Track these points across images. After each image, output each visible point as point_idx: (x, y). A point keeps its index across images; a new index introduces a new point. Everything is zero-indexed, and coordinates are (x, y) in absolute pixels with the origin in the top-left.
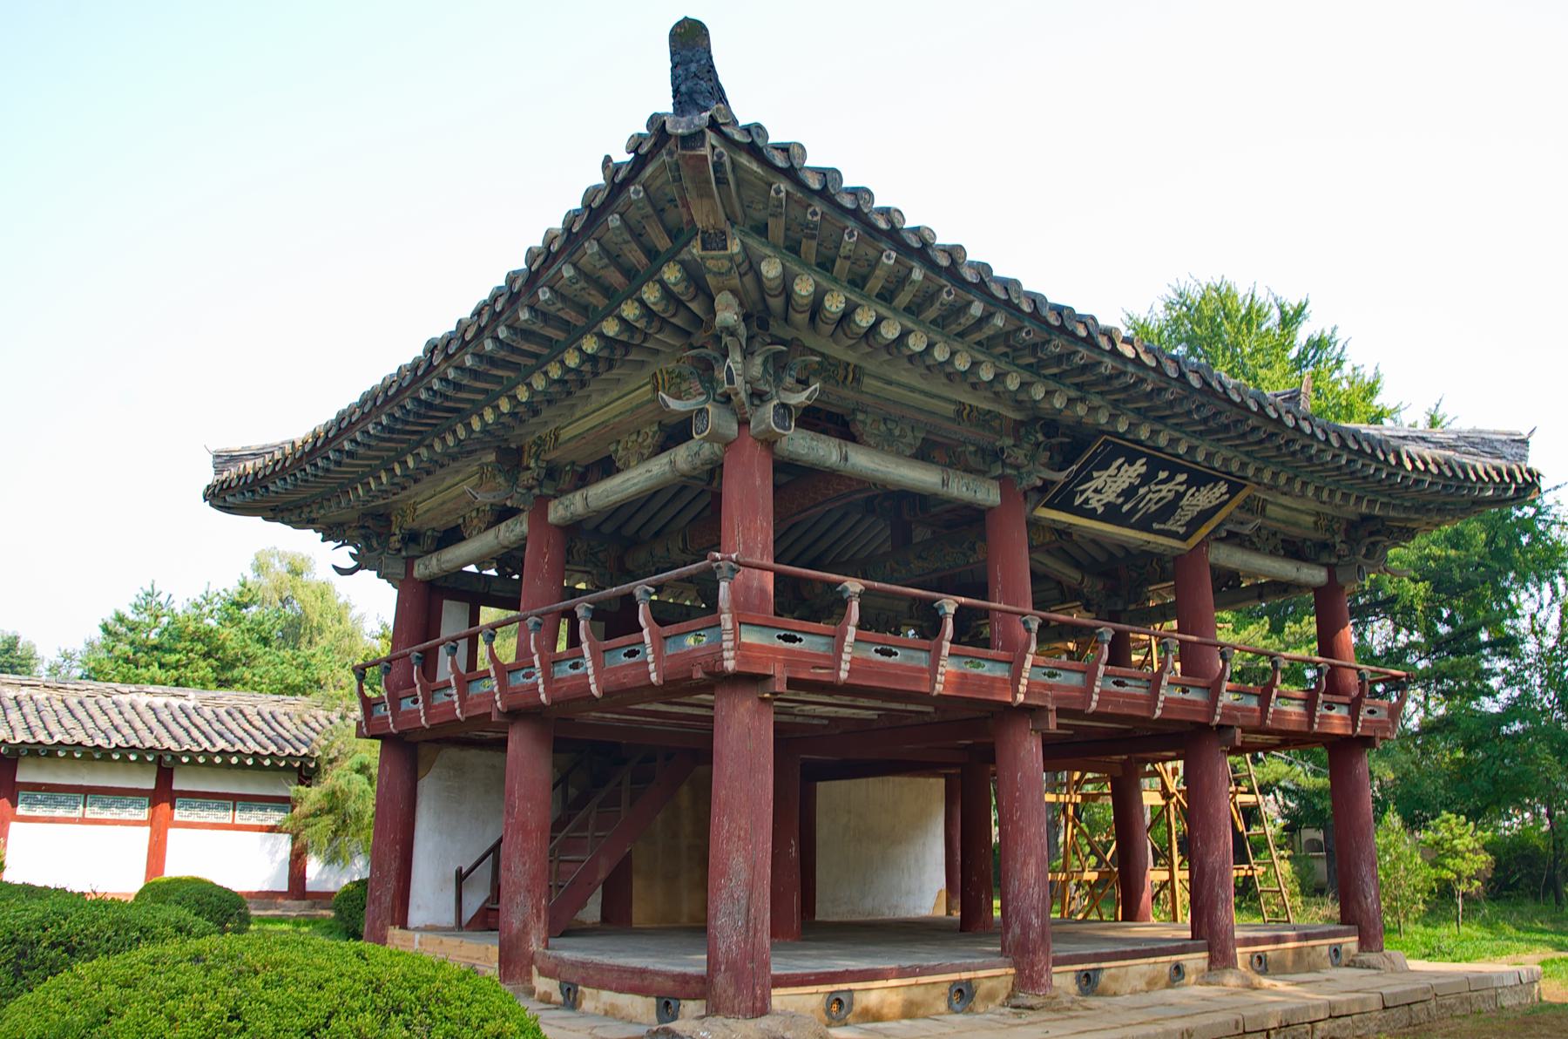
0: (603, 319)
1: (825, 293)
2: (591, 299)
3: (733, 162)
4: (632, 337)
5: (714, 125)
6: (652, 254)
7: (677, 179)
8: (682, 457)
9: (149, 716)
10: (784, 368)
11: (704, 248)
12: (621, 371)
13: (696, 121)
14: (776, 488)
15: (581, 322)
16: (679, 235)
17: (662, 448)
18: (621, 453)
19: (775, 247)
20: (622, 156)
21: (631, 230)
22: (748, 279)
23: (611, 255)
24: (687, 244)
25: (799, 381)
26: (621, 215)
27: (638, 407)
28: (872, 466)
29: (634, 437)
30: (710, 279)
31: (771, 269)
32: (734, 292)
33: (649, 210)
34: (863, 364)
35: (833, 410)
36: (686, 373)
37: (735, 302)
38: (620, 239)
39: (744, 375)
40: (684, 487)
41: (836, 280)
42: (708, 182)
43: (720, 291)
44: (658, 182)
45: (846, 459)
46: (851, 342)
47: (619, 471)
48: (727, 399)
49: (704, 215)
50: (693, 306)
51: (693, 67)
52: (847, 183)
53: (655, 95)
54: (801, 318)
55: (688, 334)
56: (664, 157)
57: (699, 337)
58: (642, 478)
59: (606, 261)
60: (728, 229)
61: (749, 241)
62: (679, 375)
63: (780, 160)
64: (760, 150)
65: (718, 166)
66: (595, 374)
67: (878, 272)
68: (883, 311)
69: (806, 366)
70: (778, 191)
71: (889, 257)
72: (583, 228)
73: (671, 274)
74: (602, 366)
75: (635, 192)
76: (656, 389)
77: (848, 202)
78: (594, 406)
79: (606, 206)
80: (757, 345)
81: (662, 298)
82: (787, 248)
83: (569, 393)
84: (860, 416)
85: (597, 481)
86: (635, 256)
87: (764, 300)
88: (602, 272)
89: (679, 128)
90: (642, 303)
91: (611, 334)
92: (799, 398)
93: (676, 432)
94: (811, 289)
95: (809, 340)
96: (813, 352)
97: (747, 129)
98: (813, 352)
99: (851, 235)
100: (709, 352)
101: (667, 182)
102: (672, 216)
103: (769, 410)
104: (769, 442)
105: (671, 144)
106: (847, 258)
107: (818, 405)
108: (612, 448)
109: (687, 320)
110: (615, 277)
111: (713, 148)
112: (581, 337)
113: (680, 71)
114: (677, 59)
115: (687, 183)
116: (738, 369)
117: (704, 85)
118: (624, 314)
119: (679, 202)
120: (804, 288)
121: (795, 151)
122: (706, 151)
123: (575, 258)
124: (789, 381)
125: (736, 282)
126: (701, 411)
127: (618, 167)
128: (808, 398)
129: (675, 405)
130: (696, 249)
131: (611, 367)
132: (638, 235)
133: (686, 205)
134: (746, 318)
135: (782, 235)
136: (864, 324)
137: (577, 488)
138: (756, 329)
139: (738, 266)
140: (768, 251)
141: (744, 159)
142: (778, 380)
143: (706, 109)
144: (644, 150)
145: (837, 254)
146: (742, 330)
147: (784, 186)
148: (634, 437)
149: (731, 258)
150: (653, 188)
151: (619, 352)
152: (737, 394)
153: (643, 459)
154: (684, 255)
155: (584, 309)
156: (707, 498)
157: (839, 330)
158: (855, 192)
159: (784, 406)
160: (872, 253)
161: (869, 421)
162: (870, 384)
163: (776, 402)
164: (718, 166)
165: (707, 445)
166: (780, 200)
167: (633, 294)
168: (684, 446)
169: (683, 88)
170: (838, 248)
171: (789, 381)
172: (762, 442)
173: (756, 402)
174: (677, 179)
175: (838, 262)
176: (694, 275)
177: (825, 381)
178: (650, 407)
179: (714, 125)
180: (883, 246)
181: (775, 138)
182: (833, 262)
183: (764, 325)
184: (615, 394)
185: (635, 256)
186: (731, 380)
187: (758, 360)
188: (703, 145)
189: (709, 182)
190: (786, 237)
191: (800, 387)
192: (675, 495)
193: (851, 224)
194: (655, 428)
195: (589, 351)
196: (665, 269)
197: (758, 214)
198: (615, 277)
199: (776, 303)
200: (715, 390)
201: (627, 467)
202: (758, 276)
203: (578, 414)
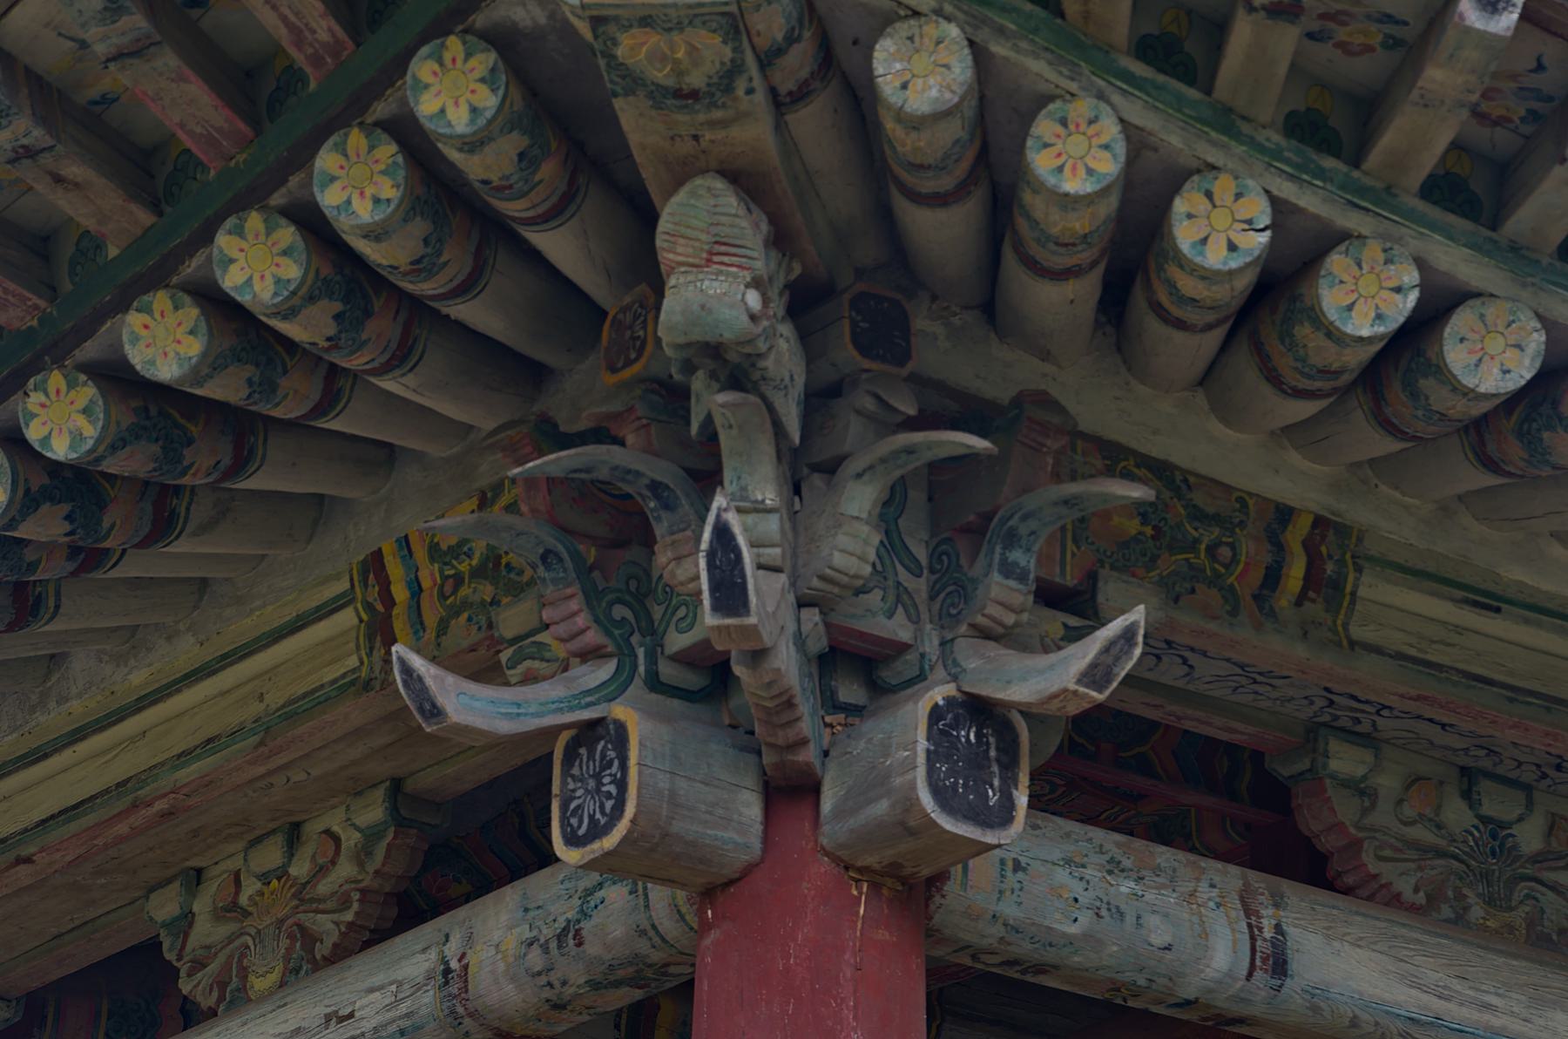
45: (1279, 966)
68: (1458, 262)
93: (475, 833)
103: (907, 731)
128: (1095, 675)
163: (939, 694)
173: (850, 691)
187: (860, 497)
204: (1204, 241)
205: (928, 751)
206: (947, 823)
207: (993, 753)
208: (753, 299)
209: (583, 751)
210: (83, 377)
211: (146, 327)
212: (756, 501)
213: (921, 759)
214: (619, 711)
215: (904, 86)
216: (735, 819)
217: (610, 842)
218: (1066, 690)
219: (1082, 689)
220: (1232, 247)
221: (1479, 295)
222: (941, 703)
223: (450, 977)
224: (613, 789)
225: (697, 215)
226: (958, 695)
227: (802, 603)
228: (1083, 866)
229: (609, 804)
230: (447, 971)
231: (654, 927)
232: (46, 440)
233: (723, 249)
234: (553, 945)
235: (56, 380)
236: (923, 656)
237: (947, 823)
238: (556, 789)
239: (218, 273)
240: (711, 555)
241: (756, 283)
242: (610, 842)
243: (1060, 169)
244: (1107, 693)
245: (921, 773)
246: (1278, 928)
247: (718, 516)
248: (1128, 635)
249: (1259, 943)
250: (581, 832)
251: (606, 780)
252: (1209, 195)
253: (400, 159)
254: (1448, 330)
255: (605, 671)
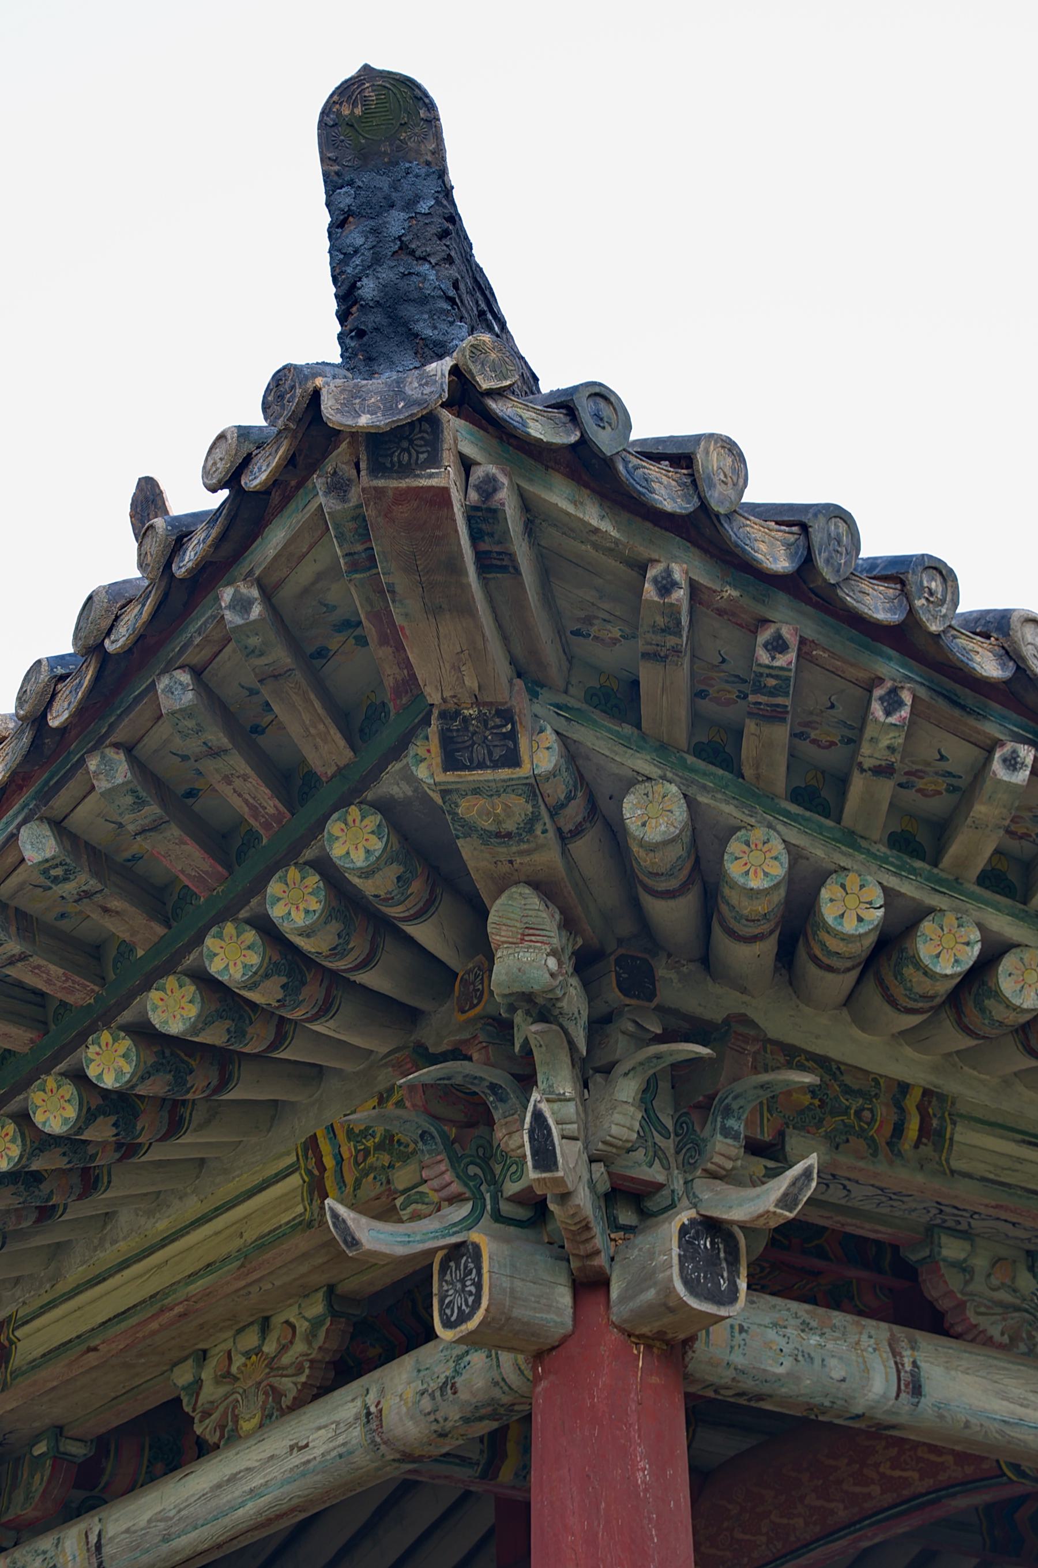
0: (146, 987)
1: (822, 877)
2: (110, 925)
3: (522, 496)
4: (239, 1034)
5: (465, 396)
6: (294, 783)
7: (364, 562)
8: (401, 1396)
10: (705, 1107)
11: (451, 763)
12: (210, 1136)
13: (413, 388)
14: (702, 1478)
15: (79, 993)
16: (374, 725)
17: (341, 1370)
18: (210, 1392)
19: (663, 749)
20: (191, 496)
21: (410, 274)
22: (587, 849)
23: (172, 795)
24: (399, 749)
25: (754, 1148)
26: (197, 673)
27: (264, 1243)
28: (1000, 1408)
29: (250, 1339)
30: (469, 850)
31: (654, 816)
32: (544, 888)
33: (280, 656)
34: (951, 1086)
35: (866, 1230)
36: (407, 1135)
37: (548, 919)
38: (193, 746)
39: (584, 1136)
40: (406, 1487)
41: (851, 839)
42: (454, 566)
43: (502, 885)
44: (306, 573)
45: (917, 1389)
46: (915, 1020)
47: (203, 1450)
48: (535, 1212)
49: (447, 661)
50: (423, 933)
51: (396, 223)
52: (874, 545)
53: (296, 318)
54: (751, 957)
55: (412, 1016)
56: (320, 496)
57: (445, 1024)
58: (275, 1472)
59: (153, 810)
60: (520, 702)
61: (585, 736)
62: (388, 1142)
63: (666, 492)
64: (607, 463)
65: (483, 519)
66: (128, 1150)
67: (980, 810)
69: (774, 1100)
70: (666, 586)
71: (1012, 763)
72: (84, 714)
73: (354, 842)
74: (147, 1127)
75: (236, 604)
76: (317, 1189)
77: (877, 604)
78: (124, 1247)
79: (148, 647)
80: (619, 1044)
81: (330, 914)
82: (699, 751)
83: (46, 1213)
84: (952, 1249)
85: (133, 1487)
86: (242, 791)
87: (635, 905)
88: (142, 845)
89: (359, 409)
90: (269, 931)
91: (175, 1027)
92: (757, 1203)
93: (384, 1320)
94: (778, 870)
95: (778, 1020)
96: (794, 1056)
97: (564, 405)
98: (794, 1056)
99: (892, 703)
100: (477, 1070)
101: (332, 572)
102: (351, 668)
103: (665, 1241)
104: (671, 1344)
105: (339, 459)
106: (883, 771)
107: (817, 1218)
108: (183, 1376)
109: (409, 980)
110: (181, 857)
111: (466, 465)
112: (81, 1040)
113: (355, 236)
114: (346, 198)
115: (391, 573)
116: (570, 1122)
117: (432, 277)
118: (215, 968)
119: (369, 629)
120: (756, 866)
121: (710, 461)
122: (446, 476)
123: (60, 802)
124: (723, 1149)
125: (548, 857)
126: (456, 1251)
127: (182, 532)
128: (787, 1200)
129: (379, 1238)
130: (425, 767)
131: (175, 1127)
132: (248, 731)
133: (392, 638)
134: (585, 963)
135: (683, 713)
136: (946, 967)
137: (70, 1512)
138: (613, 995)
139: (554, 812)
140: (642, 763)
141: (559, 496)
142: (690, 1149)
143: (440, 351)
144: (256, 478)
145: (853, 762)
146: (574, 1000)
147: (683, 567)
148: (250, 1339)
149: (532, 788)
150: (287, 592)
151: (199, 1083)
152: (565, 1197)
153: (280, 1409)
154: (391, 785)
155: (90, 955)
156: (482, 1518)
157: (870, 987)
158: (897, 573)
159: (712, 1226)
160: (960, 754)
161: (980, 1263)
162: (975, 1146)
163: (685, 1216)
164: (483, 519)
165: (478, 1359)
166: (673, 611)
167: (242, 905)
168: (407, 1362)
169: (368, 288)
170: (853, 741)
171: (723, 1149)
172: (648, 1342)
173: (626, 1217)
174: (364, 562)
175: (858, 784)
176: (424, 847)
177: (835, 1143)
178: (301, 1243)
179: (465, 396)
180: (992, 729)
181: (648, 424)
182: (842, 783)
183: (639, 982)
184: (192, 1207)
185: (242, 791)
186: (545, 1157)
187: (627, 1089)
188: (434, 460)
189: (462, 572)
190: (696, 717)
191: (759, 1165)
192: (381, 1512)
193: (890, 668)
194: (317, 1308)
195: (109, 1082)
196: (334, 827)
197: (610, 654)
198: (181, 857)
199: (674, 915)
200: (496, 1184)
201: (230, 1436)
202: (615, 834)
203: (75, 1273)
204: (842, 916)
205: (679, 1255)
206: (694, 1303)
207: (722, 1255)
208: (552, 963)
209: (452, 1264)
210: (122, 1034)
211: (162, 1000)
212: (560, 1094)
213: (675, 1261)
214: (475, 1236)
215: (644, 825)
216: (555, 1306)
217: (472, 1325)
218: (768, 1212)
219: (779, 1211)
220: (860, 919)
221: (1018, 946)
222: (687, 1222)
223: (370, 1417)
224: (473, 1289)
225: (513, 911)
226: (698, 1217)
227: (592, 1160)
228: (785, 1327)
229: (471, 1300)
230: (369, 1414)
231: (503, 1379)
232: (100, 1076)
233: (531, 932)
234: (438, 1394)
235: (106, 1036)
236: (673, 1191)
237: (694, 1303)
238: (435, 1290)
239: (207, 963)
240: (531, 1132)
241: (553, 953)
242: (472, 1325)
243: (747, 873)
244: (796, 1212)
245: (676, 1270)
246: (914, 1364)
247: (535, 1106)
248: (807, 1173)
249: (902, 1374)
250: (453, 1319)
251: (468, 1283)
252: (843, 886)
253: (321, 884)
254: (1000, 969)
255: (466, 1209)
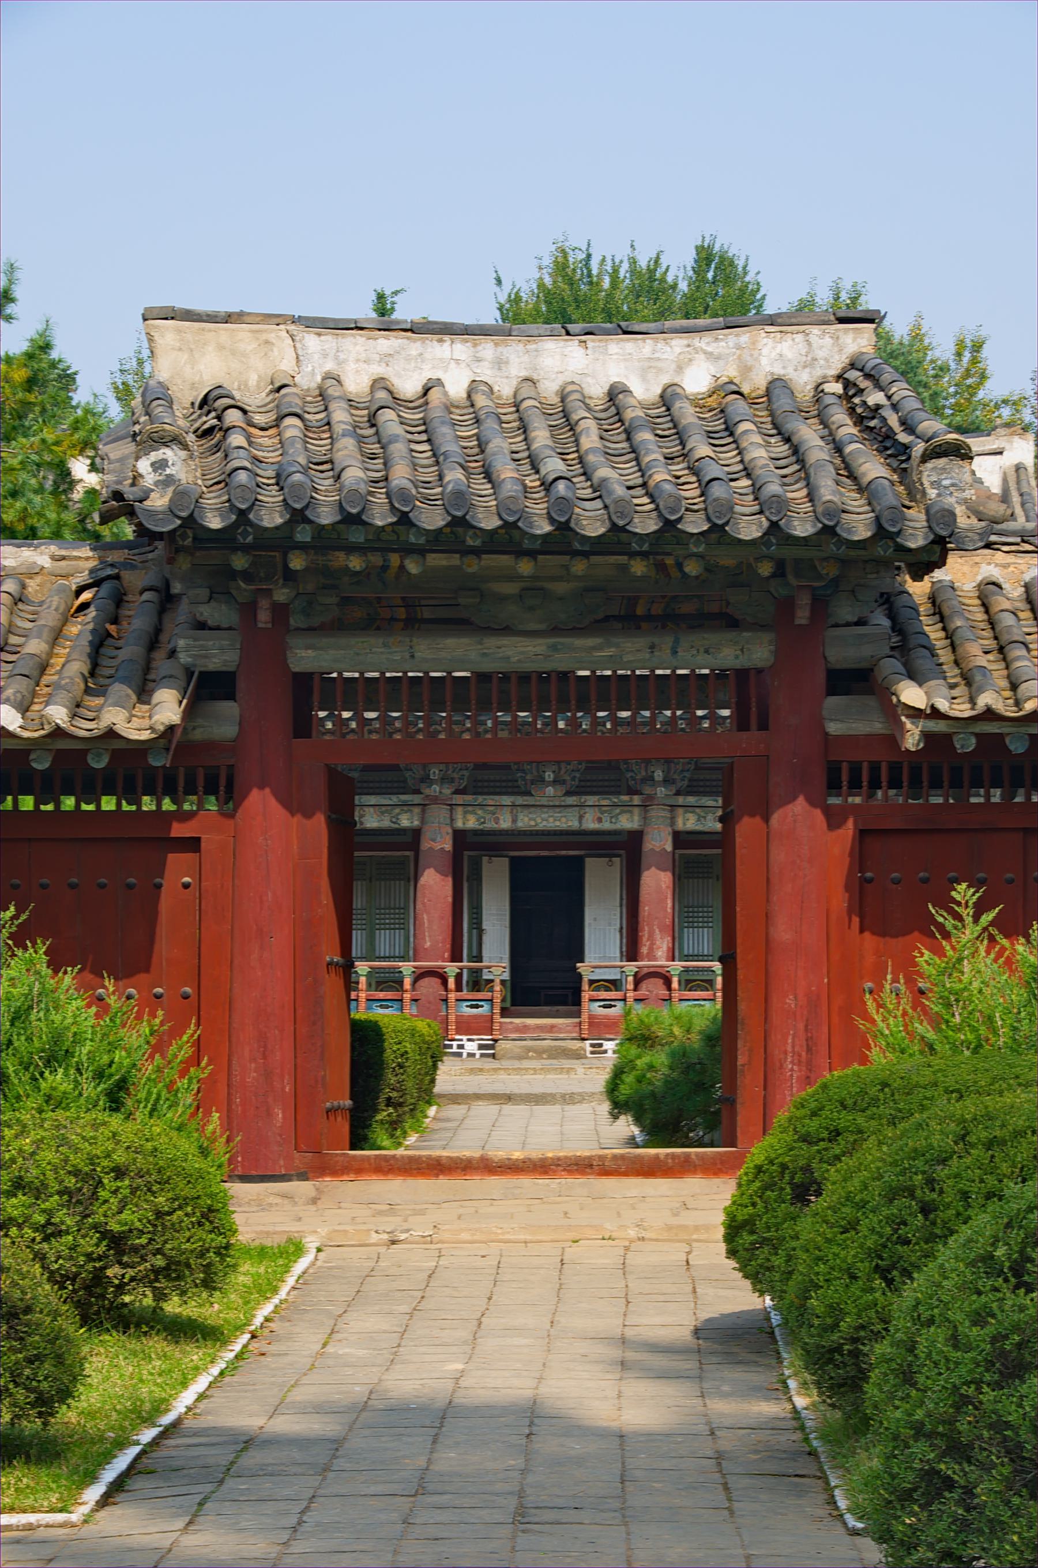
9: (583, 784)
